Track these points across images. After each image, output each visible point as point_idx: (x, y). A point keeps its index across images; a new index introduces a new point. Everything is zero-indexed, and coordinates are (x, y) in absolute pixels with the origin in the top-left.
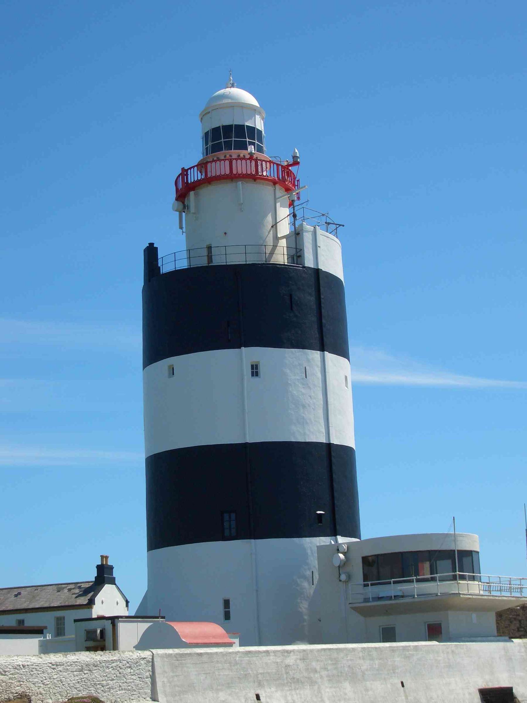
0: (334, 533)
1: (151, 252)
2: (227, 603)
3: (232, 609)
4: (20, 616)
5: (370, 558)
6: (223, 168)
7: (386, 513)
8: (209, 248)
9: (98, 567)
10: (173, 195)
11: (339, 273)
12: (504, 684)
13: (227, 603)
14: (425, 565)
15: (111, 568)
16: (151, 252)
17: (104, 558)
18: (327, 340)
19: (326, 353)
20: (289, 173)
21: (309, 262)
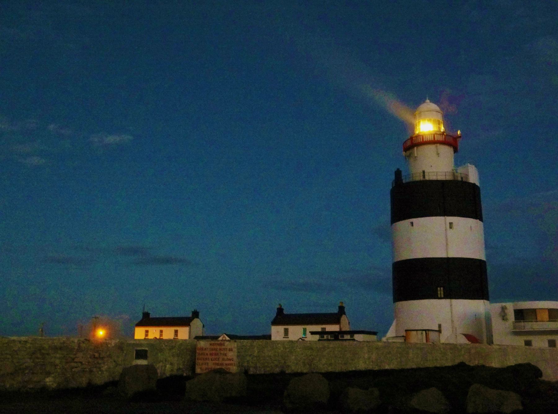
8: (424, 172)
16: (398, 173)
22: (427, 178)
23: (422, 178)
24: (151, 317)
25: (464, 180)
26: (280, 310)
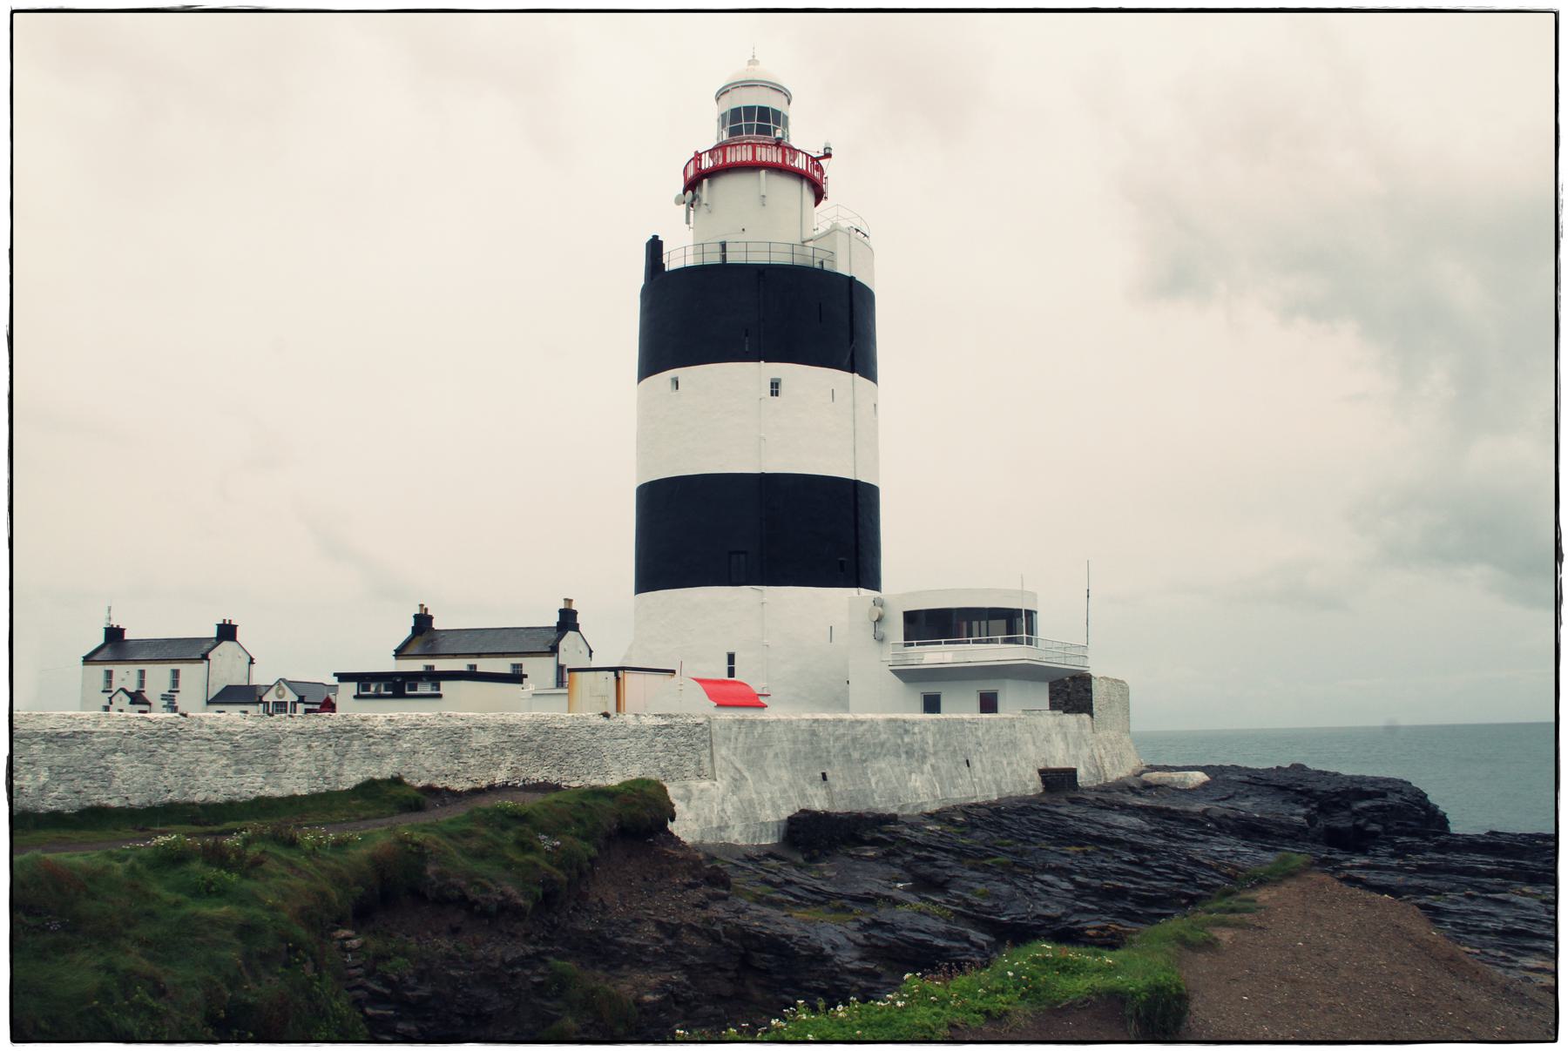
3: (737, 666)
6: (743, 155)
8: (724, 245)
9: (416, 616)
10: (680, 185)
15: (575, 613)
16: (655, 247)
17: (569, 601)
20: (819, 168)
22: (730, 260)
23: (717, 260)
24: (436, 625)
25: (827, 267)
26: (423, 622)
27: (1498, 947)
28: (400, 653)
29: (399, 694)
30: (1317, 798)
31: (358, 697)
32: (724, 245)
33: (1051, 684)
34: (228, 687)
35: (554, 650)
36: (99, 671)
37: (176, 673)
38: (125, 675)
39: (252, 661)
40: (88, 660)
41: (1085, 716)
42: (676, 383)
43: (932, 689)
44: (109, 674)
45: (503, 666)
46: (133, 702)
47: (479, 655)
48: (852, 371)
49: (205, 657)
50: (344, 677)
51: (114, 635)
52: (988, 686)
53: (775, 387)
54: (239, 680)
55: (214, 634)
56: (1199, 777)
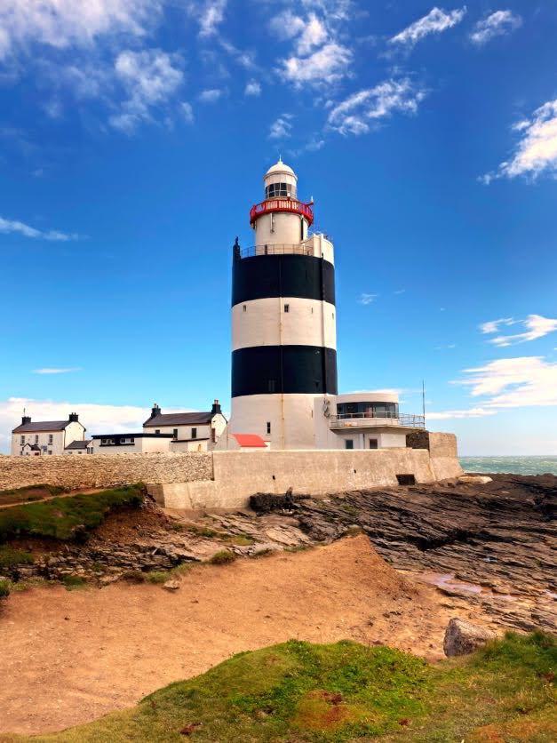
0: (324, 392)
1: (236, 249)
2: (269, 425)
4: (158, 429)
5: (298, 85)
7: (350, 387)
8: (266, 247)
10: (249, 219)
11: (332, 262)
12: (410, 473)
13: (269, 425)
14: (547, 316)
15: (219, 406)
16: (236, 249)
18: (324, 296)
19: (324, 302)
21: (317, 254)
23: (263, 253)
24: (163, 412)
27: (123, 558)
28: (145, 426)
29: (118, 444)
30: (545, 490)
31: (101, 446)
32: (266, 247)
33: (408, 437)
34: (75, 441)
35: (209, 422)
36: (18, 436)
37: (51, 436)
38: (30, 438)
39: (85, 430)
40: (14, 432)
41: (426, 450)
42: (245, 307)
43: (349, 437)
44: (23, 437)
45: (170, 430)
46: (33, 449)
47: (179, 425)
48: (322, 299)
49: (63, 429)
50: (96, 437)
51: (26, 420)
52: (373, 437)
53: (287, 308)
54: (79, 438)
55: (68, 419)
56: (486, 480)
